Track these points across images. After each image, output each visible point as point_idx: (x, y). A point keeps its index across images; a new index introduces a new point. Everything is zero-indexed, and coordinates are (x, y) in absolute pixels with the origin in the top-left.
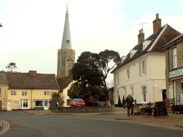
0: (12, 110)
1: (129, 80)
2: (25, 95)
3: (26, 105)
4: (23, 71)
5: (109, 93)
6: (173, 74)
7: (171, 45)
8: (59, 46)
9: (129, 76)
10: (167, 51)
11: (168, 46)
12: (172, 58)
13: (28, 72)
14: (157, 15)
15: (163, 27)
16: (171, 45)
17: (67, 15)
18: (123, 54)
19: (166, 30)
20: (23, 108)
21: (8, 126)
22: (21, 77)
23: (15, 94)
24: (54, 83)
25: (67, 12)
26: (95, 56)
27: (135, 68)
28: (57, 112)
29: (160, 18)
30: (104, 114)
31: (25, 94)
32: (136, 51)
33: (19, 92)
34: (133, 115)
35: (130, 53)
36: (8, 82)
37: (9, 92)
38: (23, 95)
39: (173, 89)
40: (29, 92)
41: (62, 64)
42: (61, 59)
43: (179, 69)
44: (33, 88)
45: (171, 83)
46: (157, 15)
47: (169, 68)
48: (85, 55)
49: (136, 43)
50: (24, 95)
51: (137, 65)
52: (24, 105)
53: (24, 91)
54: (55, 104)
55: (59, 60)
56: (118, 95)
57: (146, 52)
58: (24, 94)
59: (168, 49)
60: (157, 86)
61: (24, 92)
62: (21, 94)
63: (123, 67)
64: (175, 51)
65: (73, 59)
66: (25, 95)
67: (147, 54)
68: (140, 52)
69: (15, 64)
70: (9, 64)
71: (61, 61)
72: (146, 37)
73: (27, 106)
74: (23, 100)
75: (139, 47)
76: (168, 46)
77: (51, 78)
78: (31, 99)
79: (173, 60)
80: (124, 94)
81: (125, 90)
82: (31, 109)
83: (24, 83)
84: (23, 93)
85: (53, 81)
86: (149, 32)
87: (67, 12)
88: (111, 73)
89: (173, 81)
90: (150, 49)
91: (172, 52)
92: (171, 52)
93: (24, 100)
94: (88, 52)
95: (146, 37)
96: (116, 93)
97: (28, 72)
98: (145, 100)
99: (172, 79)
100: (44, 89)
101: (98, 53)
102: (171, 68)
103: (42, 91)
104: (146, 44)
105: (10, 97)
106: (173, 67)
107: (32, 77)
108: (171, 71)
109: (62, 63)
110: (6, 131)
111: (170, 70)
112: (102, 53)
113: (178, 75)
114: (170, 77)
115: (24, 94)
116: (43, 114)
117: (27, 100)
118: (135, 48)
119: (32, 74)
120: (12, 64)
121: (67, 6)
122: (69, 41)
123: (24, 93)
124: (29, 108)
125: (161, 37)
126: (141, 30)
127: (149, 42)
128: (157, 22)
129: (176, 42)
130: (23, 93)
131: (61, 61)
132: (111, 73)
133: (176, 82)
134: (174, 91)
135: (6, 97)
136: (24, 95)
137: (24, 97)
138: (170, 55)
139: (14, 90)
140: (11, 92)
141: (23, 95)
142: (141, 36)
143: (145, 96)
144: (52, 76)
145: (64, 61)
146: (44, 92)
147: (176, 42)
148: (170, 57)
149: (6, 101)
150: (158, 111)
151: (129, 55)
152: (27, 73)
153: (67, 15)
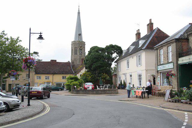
1: (128, 69)
4: (44, 60)
5: (113, 78)
6: (160, 68)
7: (159, 47)
8: (72, 38)
9: (128, 65)
10: (156, 51)
11: (157, 47)
12: (160, 56)
13: (50, 61)
14: (150, 20)
15: (154, 30)
16: (159, 47)
17: (79, 13)
18: (124, 48)
19: (156, 32)
21: (48, 108)
23: (40, 78)
25: (79, 11)
26: (102, 49)
27: (133, 60)
28: (75, 94)
29: (152, 22)
30: (110, 95)
32: (134, 47)
33: (43, 77)
34: (133, 85)
35: (129, 48)
38: (46, 79)
39: (161, 78)
40: (51, 76)
43: (164, 64)
44: (54, 74)
45: (159, 74)
46: (150, 20)
47: (158, 63)
48: (95, 49)
49: (134, 39)
51: (135, 58)
53: (47, 75)
54: (73, 87)
55: (72, 50)
56: (120, 80)
57: (141, 49)
59: (157, 49)
63: (124, 59)
64: (162, 51)
67: (142, 51)
68: (136, 49)
69: (38, 53)
72: (142, 36)
75: (135, 44)
76: (157, 47)
78: (52, 82)
79: (160, 57)
80: (124, 79)
81: (126, 76)
85: (69, 68)
86: (144, 32)
87: (79, 11)
88: (115, 62)
89: (160, 73)
90: (144, 48)
91: (160, 52)
92: (159, 52)
95: (142, 36)
96: (119, 79)
97: (50, 61)
98: (140, 84)
99: (160, 72)
100: (63, 74)
102: (159, 64)
103: (60, 76)
104: (141, 42)
105: (37, 80)
106: (160, 62)
108: (159, 66)
109: (75, 52)
110: (48, 112)
111: (158, 65)
113: (163, 69)
114: (158, 70)
116: (65, 94)
118: (133, 45)
119: (53, 62)
123: (47, 77)
125: (153, 38)
127: (143, 41)
128: (150, 25)
129: (163, 45)
132: (115, 62)
133: (163, 74)
134: (161, 80)
138: (158, 53)
139: (39, 75)
141: (46, 79)
142: (138, 34)
143: (140, 82)
144: (69, 63)
147: (163, 45)
148: (159, 55)
151: (128, 49)
153: (79, 13)
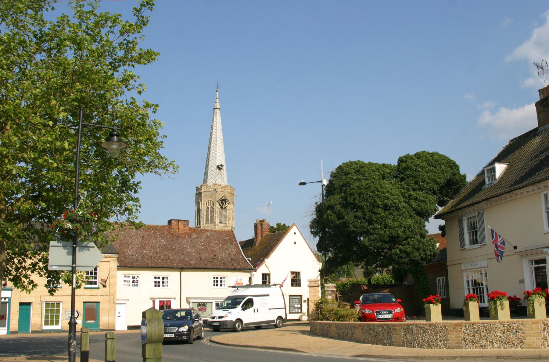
2: (221, 285)
33: (147, 277)
38: (157, 284)
40: (173, 276)
41: (207, 219)
42: (205, 207)
53: (161, 274)
58: (159, 282)
60: (88, 321)
61: (159, 278)
84: (157, 280)
115: (159, 282)
121: (303, 184)
123: (161, 280)
130: (157, 280)
131: (205, 211)
136: (159, 286)
141: (157, 284)
149: (112, 302)
150: (411, 325)
152: (164, 226)
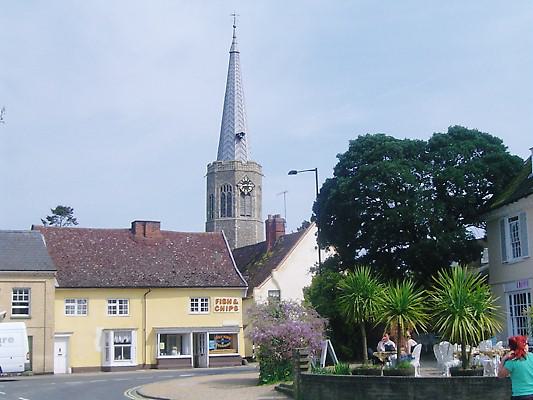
0: (73, 370)
3: (124, 352)
20: (113, 363)
22: (103, 244)
24: (226, 264)
31: (121, 307)
33: (98, 304)
36: (57, 265)
37: (60, 305)
38: (112, 310)
40: (135, 302)
41: (223, 210)
50: (115, 313)
52: (118, 352)
53: (199, 294)
55: (211, 199)
58: (115, 308)
61: (115, 302)
62: (107, 310)
65: (255, 192)
66: (121, 313)
70: (53, 212)
71: (217, 193)
73: (127, 355)
74: (112, 333)
77: (213, 247)
82: (144, 366)
83: (114, 268)
93: (117, 332)
94: (381, 138)
101: (426, 140)
107: (144, 243)
109: (223, 205)
112: (438, 142)
115: (115, 308)
117: (128, 332)
120: (62, 211)
122: (243, 134)
124: (136, 360)
126: (290, 173)
130: (113, 305)
135: (48, 322)
136: (115, 313)
137: (119, 321)
140: (67, 301)
145: (230, 200)
146: (192, 300)
152: (122, 232)
